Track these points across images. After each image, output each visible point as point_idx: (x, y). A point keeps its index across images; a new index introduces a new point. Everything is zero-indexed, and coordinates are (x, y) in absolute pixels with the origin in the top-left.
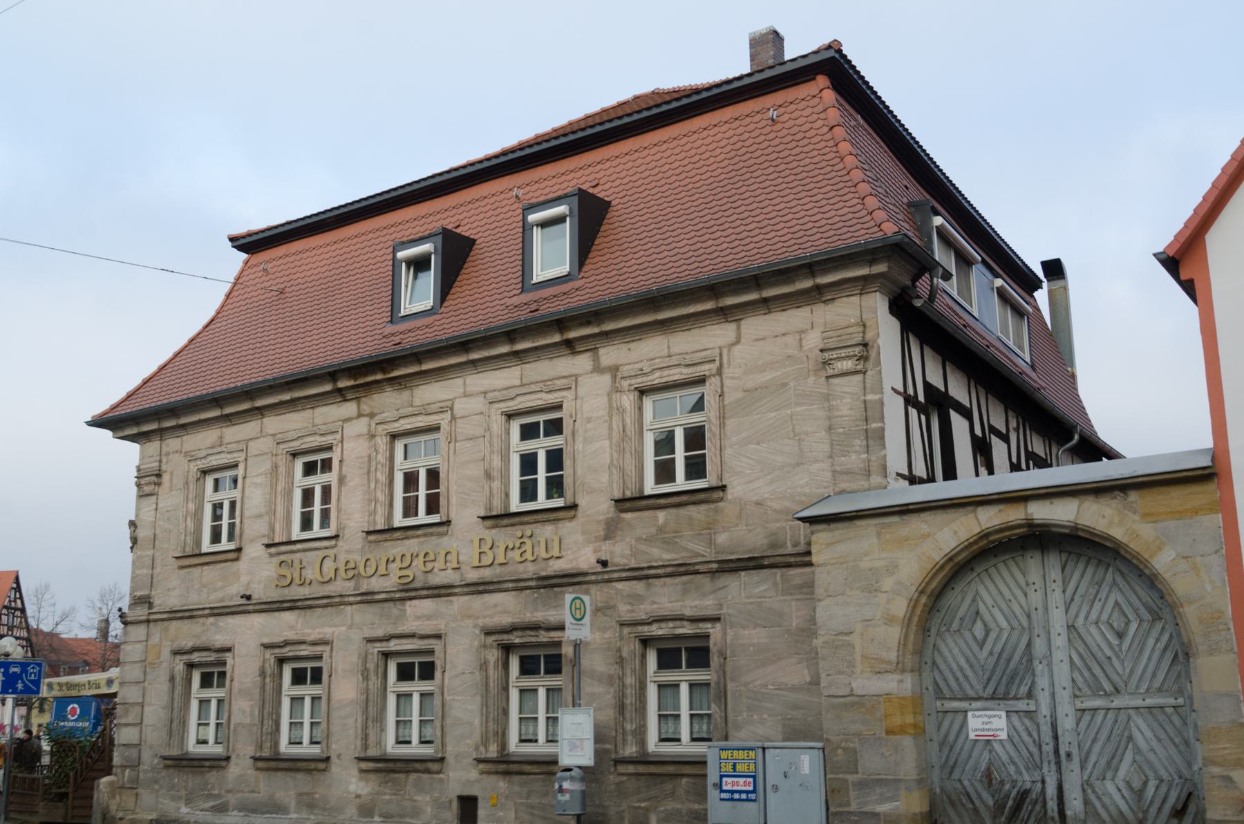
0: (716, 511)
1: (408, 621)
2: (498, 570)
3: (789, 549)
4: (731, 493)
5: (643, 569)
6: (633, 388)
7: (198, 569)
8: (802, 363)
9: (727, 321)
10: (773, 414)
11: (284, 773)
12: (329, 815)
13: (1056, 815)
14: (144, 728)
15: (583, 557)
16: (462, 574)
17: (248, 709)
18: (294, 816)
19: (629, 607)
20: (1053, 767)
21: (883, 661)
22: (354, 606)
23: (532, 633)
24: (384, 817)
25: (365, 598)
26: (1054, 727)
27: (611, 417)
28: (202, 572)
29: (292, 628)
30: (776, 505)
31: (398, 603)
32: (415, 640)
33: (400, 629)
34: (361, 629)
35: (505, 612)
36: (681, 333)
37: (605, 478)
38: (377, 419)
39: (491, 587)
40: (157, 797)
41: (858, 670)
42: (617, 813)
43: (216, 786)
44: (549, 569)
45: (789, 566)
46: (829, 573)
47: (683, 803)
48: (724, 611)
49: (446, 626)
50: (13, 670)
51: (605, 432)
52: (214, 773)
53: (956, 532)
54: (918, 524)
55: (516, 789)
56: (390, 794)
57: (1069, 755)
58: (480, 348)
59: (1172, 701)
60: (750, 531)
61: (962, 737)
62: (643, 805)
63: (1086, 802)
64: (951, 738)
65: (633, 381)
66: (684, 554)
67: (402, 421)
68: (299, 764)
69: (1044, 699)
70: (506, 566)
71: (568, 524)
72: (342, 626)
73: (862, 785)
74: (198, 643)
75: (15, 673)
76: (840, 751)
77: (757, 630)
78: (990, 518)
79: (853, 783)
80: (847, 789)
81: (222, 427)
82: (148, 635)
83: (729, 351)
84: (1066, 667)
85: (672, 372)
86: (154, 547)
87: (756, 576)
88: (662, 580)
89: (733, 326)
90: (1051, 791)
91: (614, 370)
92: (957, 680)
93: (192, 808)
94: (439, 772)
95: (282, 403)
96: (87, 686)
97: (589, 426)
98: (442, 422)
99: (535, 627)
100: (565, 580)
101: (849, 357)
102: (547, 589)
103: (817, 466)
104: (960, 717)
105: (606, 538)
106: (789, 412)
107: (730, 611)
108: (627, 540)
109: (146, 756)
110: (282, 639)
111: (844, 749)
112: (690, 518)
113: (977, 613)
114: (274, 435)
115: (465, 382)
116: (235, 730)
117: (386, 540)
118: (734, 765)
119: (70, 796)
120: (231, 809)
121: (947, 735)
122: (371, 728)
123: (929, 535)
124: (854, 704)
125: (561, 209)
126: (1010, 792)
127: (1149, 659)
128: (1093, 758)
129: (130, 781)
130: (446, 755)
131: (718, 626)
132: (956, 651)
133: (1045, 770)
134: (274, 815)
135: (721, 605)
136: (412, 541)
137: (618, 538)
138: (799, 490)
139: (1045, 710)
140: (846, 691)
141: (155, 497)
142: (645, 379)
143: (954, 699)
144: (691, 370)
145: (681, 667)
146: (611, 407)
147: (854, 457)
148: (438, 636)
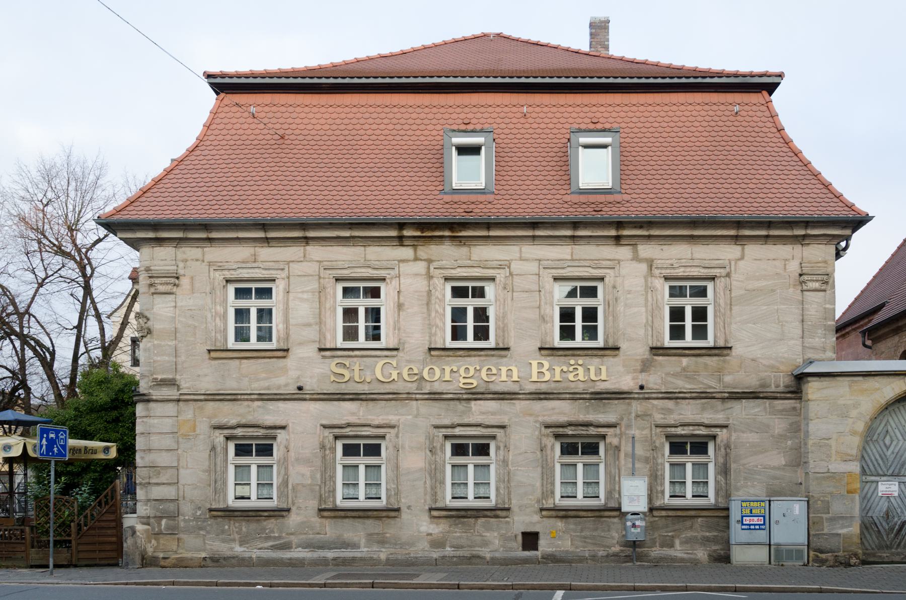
0: (724, 361)
2: (553, 385)
3: (773, 389)
4: (734, 352)
6: (662, 275)
7: (237, 362)
8: (785, 279)
10: (765, 307)
11: (352, 519)
12: (401, 548)
14: (181, 487)
15: (627, 383)
16: (521, 386)
17: (308, 474)
18: (366, 549)
19: (663, 416)
21: (848, 455)
22: (419, 402)
23: (583, 428)
25: (433, 396)
27: (647, 293)
28: (240, 365)
29: (353, 414)
30: (765, 362)
32: (479, 428)
33: (466, 421)
37: (642, 332)
38: (435, 264)
39: (551, 396)
41: (833, 459)
42: (650, 539)
43: (275, 530)
44: (596, 388)
45: (776, 398)
47: (698, 532)
48: (731, 422)
49: (509, 420)
52: (273, 520)
53: (893, 389)
55: (572, 526)
56: (460, 532)
58: (546, 228)
60: (747, 376)
61: (875, 494)
62: (670, 534)
64: (869, 495)
65: (663, 271)
66: (701, 386)
67: (459, 270)
68: (370, 513)
70: (560, 383)
71: (611, 359)
72: (409, 415)
73: (832, 520)
75: (52, 438)
77: (753, 434)
79: (826, 519)
85: (693, 270)
86: (176, 339)
89: (739, 248)
91: (650, 263)
92: (874, 465)
93: (247, 548)
95: (338, 238)
96: (83, 452)
97: (629, 296)
98: (498, 276)
99: (587, 425)
100: (613, 396)
101: (817, 281)
103: (793, 342)
104: (874, 485)
105: (642, 371)
106: (776, 307)
107: (735, 422)
111: (822, 501)
112: (706, 365)
113: (887, 431)
115: (521, 249)
116: (293, 488)
117: (448, 356)
118: (751, 510)
119: (73, 542)
120: (294, 547)
121: (867, 494)
122: (438, 488)
123: (878, 389)
124: (828, 477)
125: (607, 140)
126: (897, 522)
129: (167, 528)
130: (512, 506)
131: (725, 430)
132: (874, 450)
134: (343, 550)
136: (473, 359)
138: (781, 355)
140: (826, 470)
142: (672, 271)
143: (872, 475)
144: (706, 271)
145: (687, 454)
146: (646, 286)
147: (817, 339)
148: (503, 427)
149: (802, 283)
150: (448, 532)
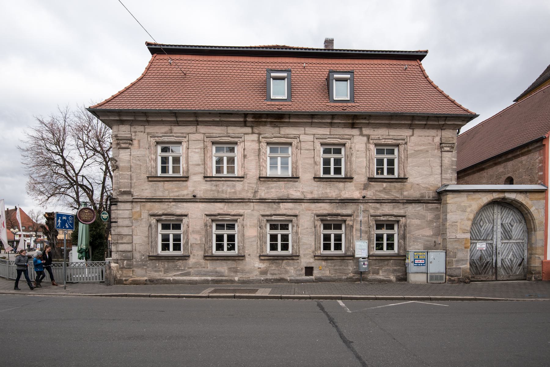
0: (404, 185)
1: (281, 210)
3: (427, 198)
5: (380, 200)
6: (374, 143)
7: (162, 183)
9: (410, 128)
10: (424, 159)
11: (221, 261)
13: (495, 267)
14: (134, 245)
15: (357, 195)
17: (199, 238)
19: (374, 211)
20: (495, 256)
21: (466, 230)
22: (254, 203)
24: (272, 274)
26: (496, 247)
29: (221, 209)
30: (423, 186)
31: (276, 204)
33: (278, 213)
34: (259, 211)
35: (325, 209)
36: (448, 130)
37: (364, 170)
38: (262, 136)
40: (146, 271)
41: (458, 232)
45: (429, 203)
46: (452, 206)
48: (407, 214)
49: (299, 213)
50: (64, 218)
51: (365, 156)
54: (478, 195)
55: (329, 264)
57: (499, 253)
58: (318, 118)
59: (522, 241)
60: (415, 192)
62: (377, 268)
63: (502, 263)
65: (374, 141)
66: (392, 197)
67: (274, 139)
69: (495, 240)
71: (349, 183)
72: (249, 210)
74: (166, 212)
76: (451, 253)
77: (417, 220)
78: (496, 196)
80: (453, 262)
81: (171, 126)
82: (132, 207)
83: (410, 138)
84: (500, 233)
85: (389, 141)
87: (417, 205)
88: (386, 204)
89: (411, 130)
90: (494, 261)
92: (475, 235)
94: (298, 260)
95: (214, 121)
97: (358, 153)
98: (293, 142)
100: (350, 201)
101: (448, 147)
102: (342, 204)
103: (437, 176)
104: (475, 244)
105: (364, 189)
106: (429, 159)
108: (372, 191)
109: (137, 256)
110: (216, 213)
112: (395, 186)
113: (481, 219)
114: (204, 134)
117: (269, 181)
123: (481, 198)
127: (518, 232)
128: (504, 254)
130: (300, 254)
132: (475, 228)
133: (493, 257)
135: (406, 212)
137: (369, 190)
139: (495, 243)
141: (129, 150)
142: (379, 141)
143: (474, 240)
144: (395, 141)
146: (366, 148)
147: (448, 175)
149: (441, 148)
150: (269, 267)
